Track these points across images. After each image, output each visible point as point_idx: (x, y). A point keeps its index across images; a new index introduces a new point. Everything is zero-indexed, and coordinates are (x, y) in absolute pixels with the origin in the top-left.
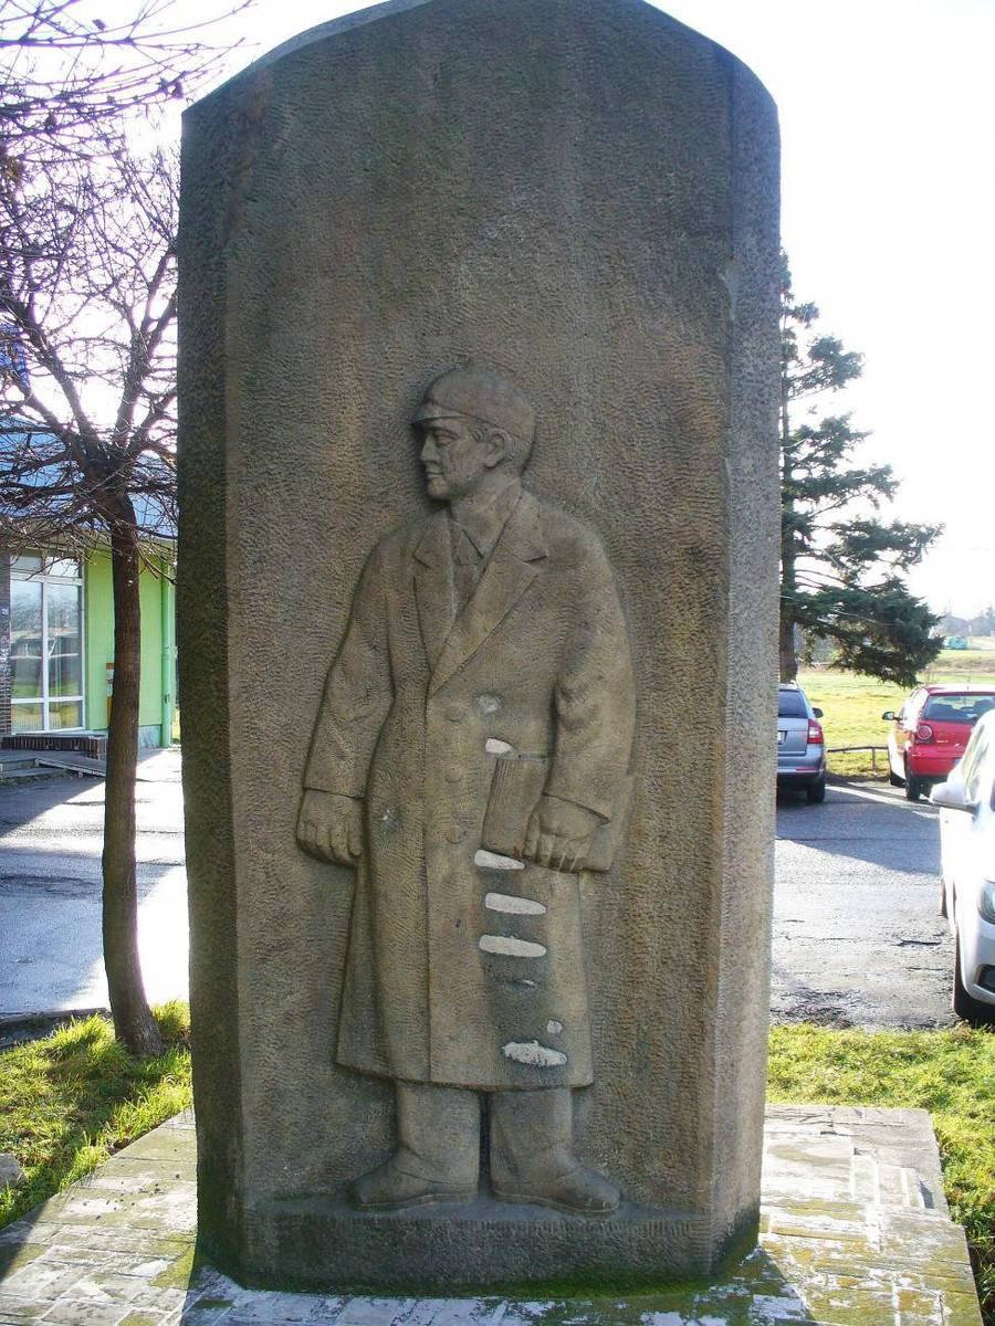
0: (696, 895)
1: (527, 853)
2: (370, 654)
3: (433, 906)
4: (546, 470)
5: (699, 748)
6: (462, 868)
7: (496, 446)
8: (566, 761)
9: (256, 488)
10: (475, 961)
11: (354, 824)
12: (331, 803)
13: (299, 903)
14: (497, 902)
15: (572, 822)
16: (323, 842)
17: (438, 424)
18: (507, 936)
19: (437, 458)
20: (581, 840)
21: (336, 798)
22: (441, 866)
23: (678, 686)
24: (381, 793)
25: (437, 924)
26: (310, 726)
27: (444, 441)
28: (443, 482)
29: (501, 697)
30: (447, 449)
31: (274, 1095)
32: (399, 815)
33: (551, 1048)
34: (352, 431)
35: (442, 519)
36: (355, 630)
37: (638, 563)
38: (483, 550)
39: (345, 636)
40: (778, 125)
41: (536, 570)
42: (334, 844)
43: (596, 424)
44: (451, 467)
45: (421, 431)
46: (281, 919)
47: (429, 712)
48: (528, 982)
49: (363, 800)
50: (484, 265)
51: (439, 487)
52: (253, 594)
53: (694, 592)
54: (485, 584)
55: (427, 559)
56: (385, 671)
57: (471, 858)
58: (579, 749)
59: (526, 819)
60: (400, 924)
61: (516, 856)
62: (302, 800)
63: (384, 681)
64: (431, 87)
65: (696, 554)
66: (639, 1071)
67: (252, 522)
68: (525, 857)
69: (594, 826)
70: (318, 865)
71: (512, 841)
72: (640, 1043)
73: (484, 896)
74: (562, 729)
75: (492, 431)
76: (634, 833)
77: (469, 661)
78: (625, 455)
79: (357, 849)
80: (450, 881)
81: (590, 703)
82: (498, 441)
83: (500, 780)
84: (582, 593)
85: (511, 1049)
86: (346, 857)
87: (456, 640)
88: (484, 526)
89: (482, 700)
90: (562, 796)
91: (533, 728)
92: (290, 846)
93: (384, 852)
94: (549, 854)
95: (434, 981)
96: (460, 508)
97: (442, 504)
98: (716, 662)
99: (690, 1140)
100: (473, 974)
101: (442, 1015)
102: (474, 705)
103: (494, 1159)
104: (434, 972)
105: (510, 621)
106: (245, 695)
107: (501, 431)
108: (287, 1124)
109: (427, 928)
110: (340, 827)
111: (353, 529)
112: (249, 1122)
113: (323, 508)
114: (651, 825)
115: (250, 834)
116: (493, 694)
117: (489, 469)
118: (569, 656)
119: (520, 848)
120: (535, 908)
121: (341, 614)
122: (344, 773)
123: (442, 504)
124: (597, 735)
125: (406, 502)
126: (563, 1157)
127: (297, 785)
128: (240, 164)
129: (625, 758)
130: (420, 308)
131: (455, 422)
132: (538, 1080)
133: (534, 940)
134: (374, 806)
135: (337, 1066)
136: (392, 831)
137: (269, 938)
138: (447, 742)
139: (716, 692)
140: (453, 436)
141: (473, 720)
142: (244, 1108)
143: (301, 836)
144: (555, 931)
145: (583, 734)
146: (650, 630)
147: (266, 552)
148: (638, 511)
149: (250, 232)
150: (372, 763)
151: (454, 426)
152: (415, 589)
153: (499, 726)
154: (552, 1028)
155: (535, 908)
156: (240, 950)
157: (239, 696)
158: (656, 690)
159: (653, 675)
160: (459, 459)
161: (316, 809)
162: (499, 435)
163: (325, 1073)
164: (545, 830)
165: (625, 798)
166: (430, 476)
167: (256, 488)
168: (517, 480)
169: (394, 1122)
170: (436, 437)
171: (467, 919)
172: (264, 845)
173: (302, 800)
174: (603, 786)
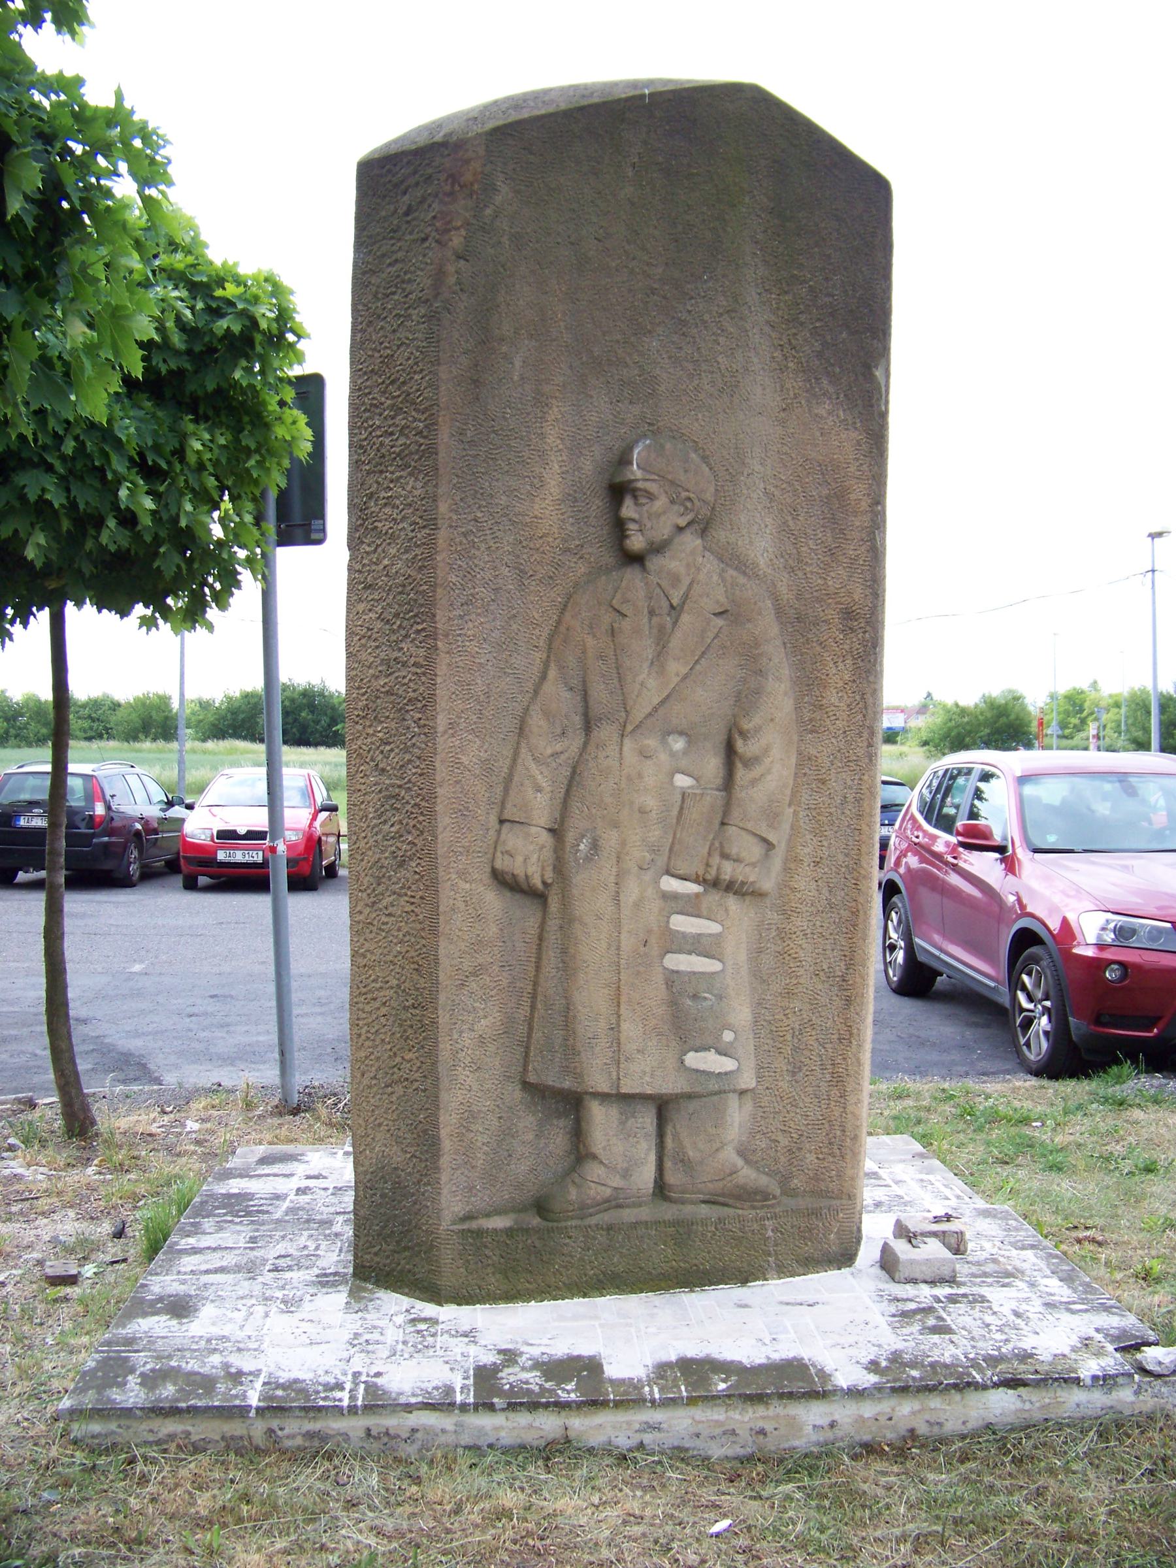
0: (845, 914)
1: (708, 877)
2: (568, 695)
3: (625, 929)
4: (721, 535)
5: (849, 783)
6: (650, 891)
7: (686, 508)
8: (743, 794)
9: (465, 535)
10: (659, 978)
11: (548, 854)
12: (528, 835)
13: (494, 929)
14: (682, 923)
15: (746, 847)
16: (519, 871)
17: (640, 485)
18: (690, 953)
19: (635, 516)
20: (754, 865)
21: (533, 830)
22: (632, 891)
23: (831, 728)
24: (577, 823)
25: (628, 943)
26: (508, 762)
27: (643, 500)
28: (641, 538)
29: (687, 735)
30: (645, 508)
31: (470, 1116)
32: (595, 846)
33: (725, 1055)
34: (554, 486)
35: (632, 575)
36: (552, 673)
37: (798, 624)
38: (675, 602)
39: (544, 677)
40: (570, 87)
41: (720, 622)
42: (530, 874)
43: (766, 493)
44: (649, 526)
45: (618, 491)
46: (478, 944)
47: (625, 749)
48: (706, 995)
49: (556, 832)
50: (673, 343)
51: (636, 542)
52: (460, 635)
53: (846, 647)
54: (678, 634)
55: (624, 609)
56: (580, 710)
57: (657, 882)
58: (754, 782)
59: (707, 847)
60: (593, 949)
61: (696, 881)
62: (499, 832)
63: (577, 720)
64: (630, 174)
65: (848, 614)
66: (794, 1074)
67: (460, 566)
68: (705, 881)
69: (763, 852)
70: (508, 894)
71: (697, 868)
72: (795, 1049)
73: (669, 917)
74: (739, 765)
75: (684, 494)
76: (792, 861)
77: (662, 702)
78: (791, 523)
79: (549, 876)
80: (637, 905)
81: (763, 742)
82: (689, 504)
83: (686, 811)
84: (757, 645)
85: (693, 1059)
86: (540, 886)
87: (652, 683)
88: (675, 579)
89: (670, 739)
90: (741, 825)
91: (713, 765)
92: (486, 877)
93: (580, 880)
94: (727, 877)
95: (623, 999)
96: (654, 563)
97: (636, 559)
98: (866, 708)
99: (838, 1133)
100: (656, 992)
101: (630, 1030)
102: (663, 742)
103: (668, 1164)
104: (624, 989)
105: (698, 667)
106: (451, 731)
107: (692, 495)
108: (479, 1144)
109: (618, 949)
110: (536, 856)
111: (551, 577)
112: (447, 1144)
113: (525, 556)
114: (805, 852)
115: (452, 865)
116: (681, 733)
117: (680, 529)
118: (746, 698)
119: (701, 873)
120: (714, 928)
121: (538, 657)
122: (540, 806)
123: (636, 559)
124: (769, 771)
125: (600, 552)
126: (729, 1155)
127: (493, 820)
128: (449, 222)
129: (788, 792)
130: (616, 377)
131: (654, 485)
132: (713, 1086)
133: (713, 957)
134: (570, 837)
135: (526, 1086)
136: (588, 859)
137: (467, 965)
138: (640, 776)
139: (865, 735)
140: (651, 497)
141: (663, 757)
142: (442, 1131)
143: (498, 865)
144: (729, 947)
145: (757, 771)
146: (808, 684)
147: (472, 595)
148: (800, 574)
149: (461, 290)
150: (568, 792)
151: (652, 487)
152: (613, 636)
153: (684, 763)
154: (728, 1036)
155: (714, 928)
156: (442, 977)
157: (445, 732)
158: (811, 732)
159: (810, 719)
160: (650, 519)
161: (513, 839)
162: (689, 499)
163: (515, 1093)
164: (725, 856)
165: (786, 827)
166: (629, 532)
167: (465, 535)
168: (699, 541)
169: (578, 1134)
170: (635, 497)
171: (653, 940)
172: (462, 874)
173: (499, 832)
174: (772, 816)
